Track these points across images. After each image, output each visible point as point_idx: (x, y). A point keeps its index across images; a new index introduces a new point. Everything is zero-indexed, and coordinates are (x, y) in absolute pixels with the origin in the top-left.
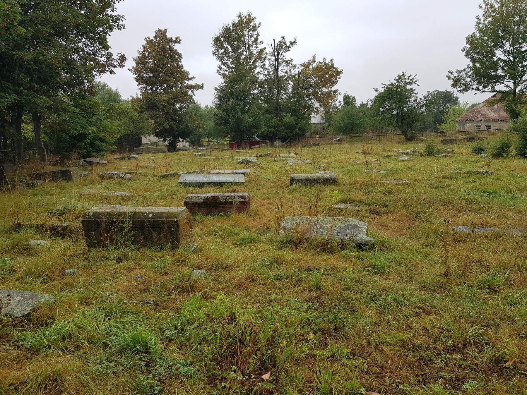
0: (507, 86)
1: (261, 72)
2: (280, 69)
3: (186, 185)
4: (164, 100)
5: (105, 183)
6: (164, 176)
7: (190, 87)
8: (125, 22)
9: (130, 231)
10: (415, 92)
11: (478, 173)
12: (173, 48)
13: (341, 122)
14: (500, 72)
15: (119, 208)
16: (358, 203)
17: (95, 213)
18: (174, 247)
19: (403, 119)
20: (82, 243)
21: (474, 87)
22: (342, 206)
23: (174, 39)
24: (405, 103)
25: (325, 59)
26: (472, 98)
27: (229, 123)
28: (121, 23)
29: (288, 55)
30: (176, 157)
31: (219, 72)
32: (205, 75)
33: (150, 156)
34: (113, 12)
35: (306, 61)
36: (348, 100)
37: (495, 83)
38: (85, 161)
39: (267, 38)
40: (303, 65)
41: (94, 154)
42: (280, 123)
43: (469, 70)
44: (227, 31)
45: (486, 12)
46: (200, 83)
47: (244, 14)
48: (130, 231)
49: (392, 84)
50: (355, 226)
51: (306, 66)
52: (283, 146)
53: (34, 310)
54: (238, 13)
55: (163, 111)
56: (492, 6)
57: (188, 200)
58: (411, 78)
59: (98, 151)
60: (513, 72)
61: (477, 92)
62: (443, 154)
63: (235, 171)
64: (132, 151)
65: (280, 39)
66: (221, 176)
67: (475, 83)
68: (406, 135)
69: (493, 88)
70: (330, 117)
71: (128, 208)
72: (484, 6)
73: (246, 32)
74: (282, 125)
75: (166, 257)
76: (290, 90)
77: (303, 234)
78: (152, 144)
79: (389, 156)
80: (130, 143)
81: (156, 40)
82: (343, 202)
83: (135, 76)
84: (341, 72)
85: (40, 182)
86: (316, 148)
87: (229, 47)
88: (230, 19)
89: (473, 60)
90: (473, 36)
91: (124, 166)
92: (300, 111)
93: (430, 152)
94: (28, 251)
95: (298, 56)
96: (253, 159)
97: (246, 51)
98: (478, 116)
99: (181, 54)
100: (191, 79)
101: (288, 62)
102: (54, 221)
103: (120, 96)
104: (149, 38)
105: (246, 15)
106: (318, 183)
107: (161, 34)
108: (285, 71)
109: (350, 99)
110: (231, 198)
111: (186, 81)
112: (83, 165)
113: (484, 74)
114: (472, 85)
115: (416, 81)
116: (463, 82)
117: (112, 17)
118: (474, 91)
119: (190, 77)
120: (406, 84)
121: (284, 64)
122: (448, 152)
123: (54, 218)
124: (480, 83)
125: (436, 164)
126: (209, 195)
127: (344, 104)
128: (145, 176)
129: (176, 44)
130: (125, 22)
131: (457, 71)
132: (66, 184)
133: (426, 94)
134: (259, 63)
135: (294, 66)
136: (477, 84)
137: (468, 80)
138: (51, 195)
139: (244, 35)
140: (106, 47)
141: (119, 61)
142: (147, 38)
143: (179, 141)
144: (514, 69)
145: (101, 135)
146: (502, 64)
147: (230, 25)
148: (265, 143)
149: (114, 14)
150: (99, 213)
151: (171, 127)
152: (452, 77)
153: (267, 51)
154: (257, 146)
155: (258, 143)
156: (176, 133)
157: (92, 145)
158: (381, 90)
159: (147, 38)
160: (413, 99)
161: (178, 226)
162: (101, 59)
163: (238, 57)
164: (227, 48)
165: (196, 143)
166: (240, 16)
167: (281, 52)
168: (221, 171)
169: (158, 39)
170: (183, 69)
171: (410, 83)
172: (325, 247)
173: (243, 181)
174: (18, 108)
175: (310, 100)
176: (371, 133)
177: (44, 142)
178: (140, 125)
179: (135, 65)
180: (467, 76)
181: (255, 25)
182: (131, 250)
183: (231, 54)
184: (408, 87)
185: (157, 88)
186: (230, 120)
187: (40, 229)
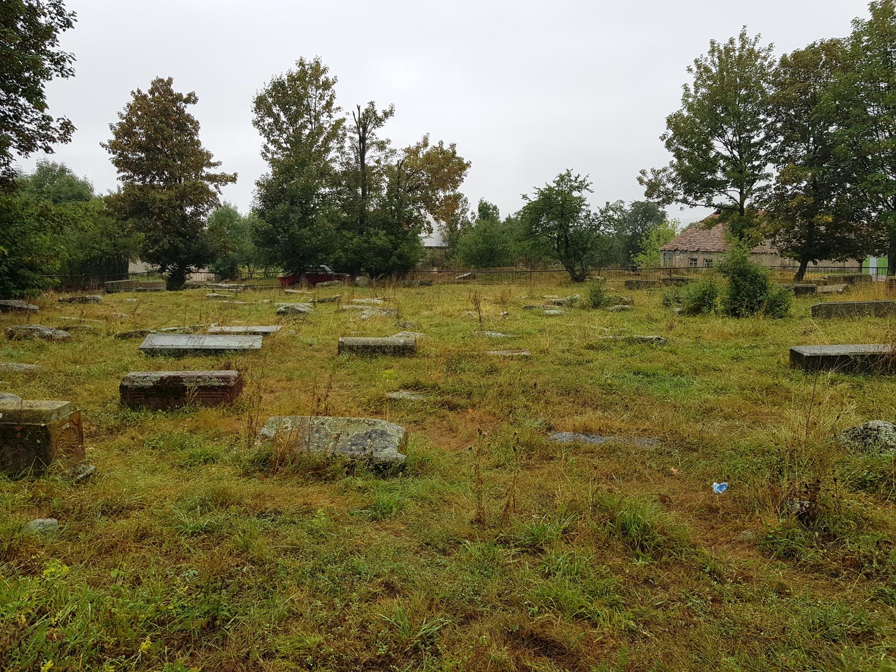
0: (731, 198)
1: (338, 157)
2: (368, 155)
3: (152, 352)
4: (161, 200)
6: (124, 336)
7: (212, 178)
8: (74, 66)
10: (586, 203)
11: (644, 341)
12: (183, 112)
13: (473, 247)
14: (719, 175)
16: (429, 389)
18: (38, 474)
19: (567, 246)
21: (680, 197)
22: (404, 394)
23: (185, 96)
24: (572, 220)
25: (441, 143)
26: (684, 215)
27: (278, 242)
29: (380, 133)
31: (264, 155)
32: (239, 161)
34: (53, 46)
35: (413, 145)
36: (486, 211)
37: (711, 192)
39: (347, 104)
40: (408, 150)
42: (366, 245)
43: (672, 170)
44: (278, 86)
45: (698, 79)
46: (230, 173)
47: (309, 60)
50: (383, 434)
51: (412, 152)
52: (370, 285)
54: (298, 59)
56: (707, 70)
57: (126, 383)
58: (579, 180)
60: (738, 175)
61: (684, 205)
63: (250, 329)
65: (367, 106)
67: (682, 192)
68: (572, 272)
69: (709, 199)
70: (457, 239)
72: (695, 69)
73: (312, 91)
74: (370, 249)
76: (384, 192)
77: (291, 447)
79: (531, 307)
80: (100, 270)
81: (154, 95)
82: (406, 387)
84: (468, 165)
86: (423, 290)
87: (282, 114)
88: (284, 67)
89: (679, 155)
90: (678, 115)
92: (401, 227)
93: (597, 302)
95: (399, 137)
96: (302, 306)
97: (311, 123)
98: (694, 244)
99: (198, 122)
100: (215, 165)
101: (381, 146)
103: (92, 190)
104: (139, 91)
105: (312, 62)
106: (384, 353)
107: (162, 87)
108: (377, 158)
109: (489, 209)
110: (205, 381)
111: (205, 168)
113: (695, 179)
114: (677, 194)
115: (588, 185)
116: (662, 189)
118: (680, 204)
119: (212, 161)
120: (572, 188)
121: (375, 147)
122: (625, 303)
124: (688, 191)
125: (598, 325)
126: (165, 374)
128: (96, 335)
129: (188, 105)
131: (653, 171)
133: (603, 206)
134: (333, 144)
135: (393, 152)
136: (685, 193)
137: (670, 186)
139: (307, 95)
140: (41, 106)
141: (62, 132)
142: (135, 91)
143: (190, 271)
144: (741, 172)
146: (722, 163)
147: (285, 77)
148: (339, 278)
151: (176, 248)
152: (646, 180)
154: (325, 283)
155: (329, 278)
158: (534, 198)
159: (135, 91)
160: (584, 214)
161: (48, 436)
162: (30, 127)
163: (298, 132)
164: (278, 115)
165: (227, 273)
166: (301, 64)
167: (369, 128)
168: (227, 329)
169: (157, 94)
170: (202, 147)
171: (579, 188)
172: (320, 472)
175: (418, 209)
176: (521, 267)
178: (121, 241)
180: (669, 180)
181: (327, 79)
183: (285, 126)
184: (575, 194)
185: (154, 178)
186: (279, 237)
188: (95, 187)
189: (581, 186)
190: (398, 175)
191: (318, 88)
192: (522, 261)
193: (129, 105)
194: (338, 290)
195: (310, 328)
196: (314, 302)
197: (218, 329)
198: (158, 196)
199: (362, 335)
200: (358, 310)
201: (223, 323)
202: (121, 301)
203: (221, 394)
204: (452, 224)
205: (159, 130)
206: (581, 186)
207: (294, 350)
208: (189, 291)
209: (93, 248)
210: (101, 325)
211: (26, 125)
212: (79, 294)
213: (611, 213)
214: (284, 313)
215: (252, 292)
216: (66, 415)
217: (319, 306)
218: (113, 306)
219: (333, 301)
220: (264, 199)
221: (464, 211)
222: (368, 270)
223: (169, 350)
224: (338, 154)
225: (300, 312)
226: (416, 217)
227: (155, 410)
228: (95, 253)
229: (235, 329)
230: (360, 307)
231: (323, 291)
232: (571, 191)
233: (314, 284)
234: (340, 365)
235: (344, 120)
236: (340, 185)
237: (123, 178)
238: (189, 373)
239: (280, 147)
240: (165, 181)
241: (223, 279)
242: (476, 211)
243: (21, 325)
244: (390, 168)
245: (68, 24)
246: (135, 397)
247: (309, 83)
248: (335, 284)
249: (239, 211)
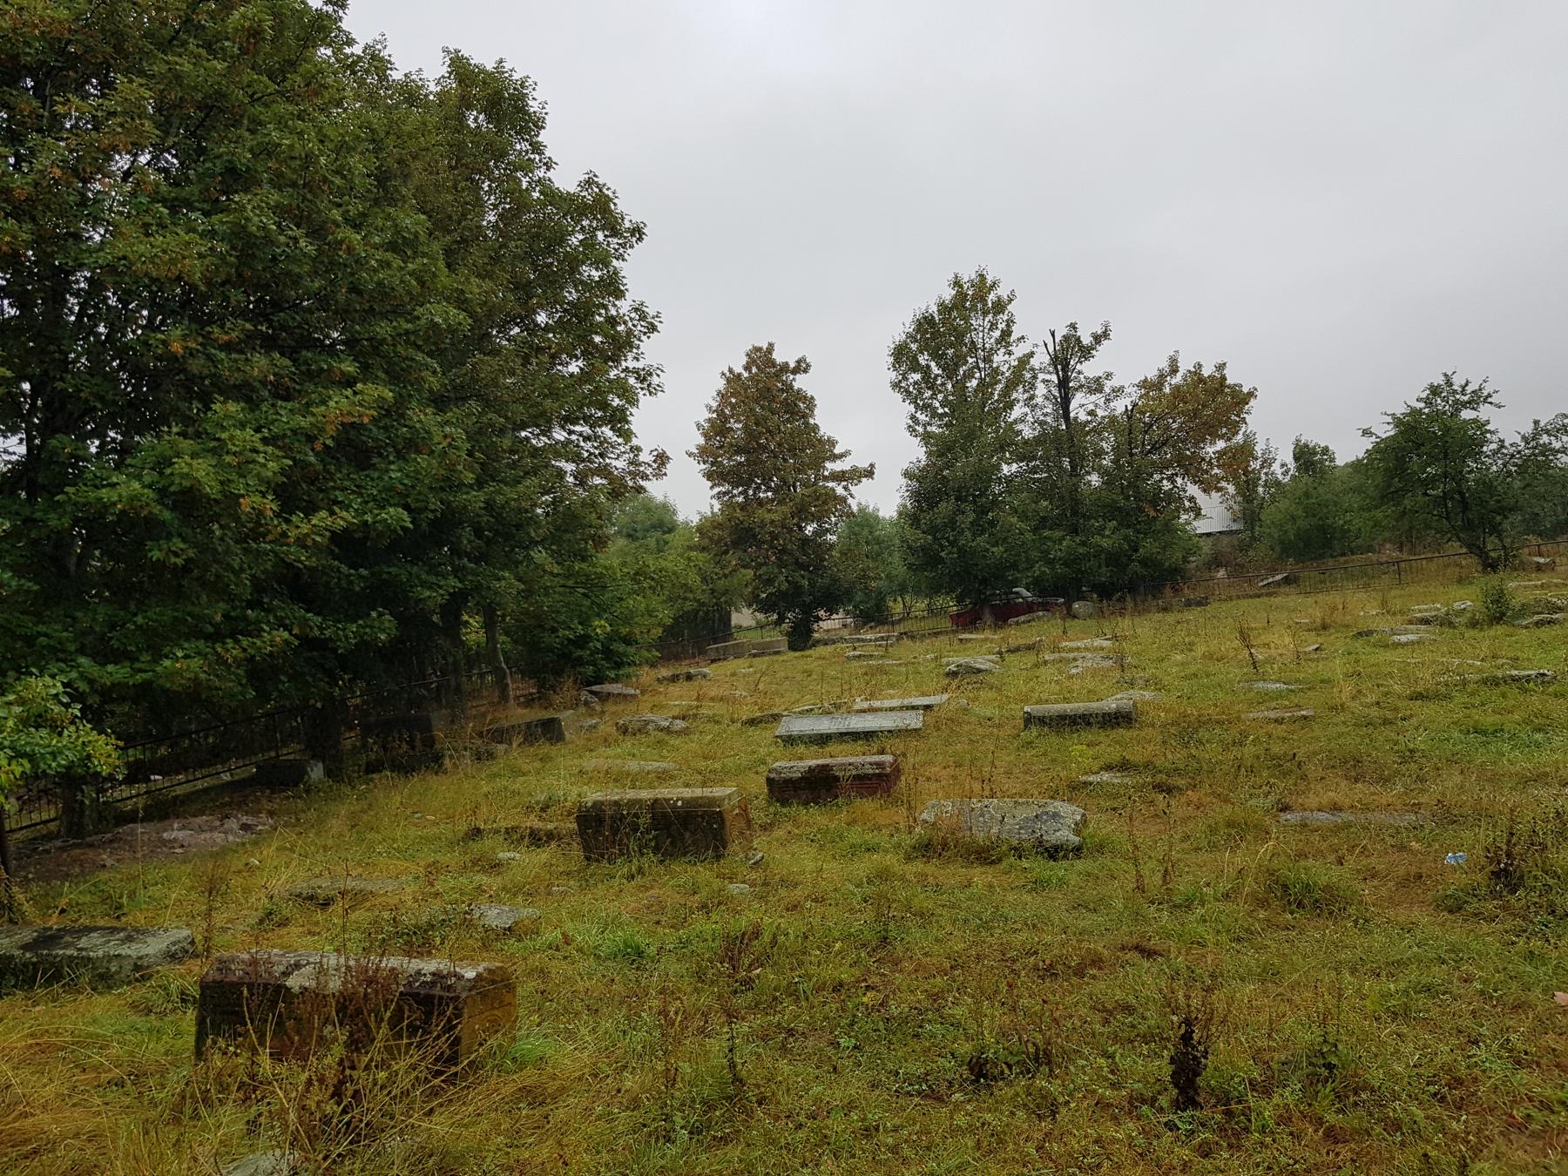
1: (1027, 416)
2: (1073, 405)
3: (790, 740)
4: (773, 522)
5: (628, 744)
6: (752, 722)
7: (839, 477)
9: (648, 831)
12: (791, 387)
15: (631, 794)
17: (595, 804)
18: (718, 857)
20: (577, 852)
22: (1106, 776)
23: (792, 365)
27: (942, 560)
28: (655, 380)
29: (1089, 369)
32: (876, 446)
35: (1152, 374)
36: (1307, 457)
38: (591, 692)
39: (1035, 329)
40: (1145, 384)
41: (612, 674)
44: (925, 324)
46: (863, 464)
48: (648, 831)
49: (1415, 412)
50: (1056, 815)
51: (1150, 386)
53: (516, 923)
55: (772, 547)
59: (618, 665)
62: (1536, 618)
63: (906, 702)
65: (1065, 331)
66: (869, 717)
71: (645, 794)
75: (703, 873)
80: (698, 633)
82: (1109, 768)
83: (703, 466)
84: (1251, 394)
85: (502, 747)
87: (933, 364)
88: (932, 294)
92: (1141, 510)
94: (496, 867)
95: (1125, 368)
96: (981, 662)
100: (841, 456)
101: (1096, 386)
102: (533, 822)
103: (674, 512)
104: (731, 370)
106: (1089, 724)
107: (761, 358)
109: (1315, 454)
112: (586, 703)
115: (1489, 396)
117: (636, 371)
119: (837, 451)
120: (1459, 406)
123: (532, 817)
126: (813, 763)
127: (1298, 469)
128: (717, 722)
130: (664, 379)
133: (1528, 429)
134: (1019, 394)
135: (1118, 391)
138: (524, 774)
140: (627, 435)
143: (818, 619)
145: (624, 631)
148: (1045, 607)
149: (639, 365)
150: (602, 803)
153: (1035, 362)
154: (1022, 618)
155: (1029, 608)
156: (808, 599)
157: (608, 653)
158: (1386, 431)
161: (723, 820)
163: (960, 387)
164: (928, 366)
165: (873, 615)
166: (957, 283)
168: (877, 704)
169: (754, 370)
172: (984, 855)
173: (919, 725)
174: (457, 602)
175: (1171, 479)
176: (1390, 552)
177: (505, 653)
179: (702, 441)
182: (649, 860)
184: (1467, 414)
187: (512, 836)
188: (679, 508)
189: (1477, 399)
190: (1129, 427)
191: (985, 314)
192: (1390, 541)
193: (719, 393)
194: (1041, 629)
195: (992, 694)
196: (1000, 653)
197: (865, 705)
198: (768, 517)
199: (1066, 700)
200: (1068, 661)
201: (872, 696)
202: (734, 674)
203: (877, 783)
204: (1247, 488)
205: (765, 420)
206: (1477, 399)
207: (966, 728)
208: (821, 650)
209: (685, 599)
210: (719, 709)
211: (614, 463)
212: (683, 668)
213: (1545, 439)
214: (954, 674)
216: (735, 801)
217: (1009, 658)
218: (727, 679)
219: (1030, 648)
220: (917, 496)
221: (1267, 463)
222: (1095, 587)
223: (810, 737)
224: (1027, 410)
225: (979, 671)
226: (1169, 494)
227: (806, 804)
228: (689, 606)
229: (887, 704)
230: (1071, 655)
231: (1016, 634)
232: (1458, 410)
233: (1005, 621)
234: (1029, 744)
235: (1032, 354)
236: (1034, 458)
237: (719, 496)
238: (839, 760)
239: (934, 414)
240: (775, 491)
241: (865, 624)
242: (1290, 460)
243: (627, 715)
244: (1113, 419)
245: (652, 328)
246: (784, 790)
247: (970, 310)
248: (1039, 618)
249: (881, 514)
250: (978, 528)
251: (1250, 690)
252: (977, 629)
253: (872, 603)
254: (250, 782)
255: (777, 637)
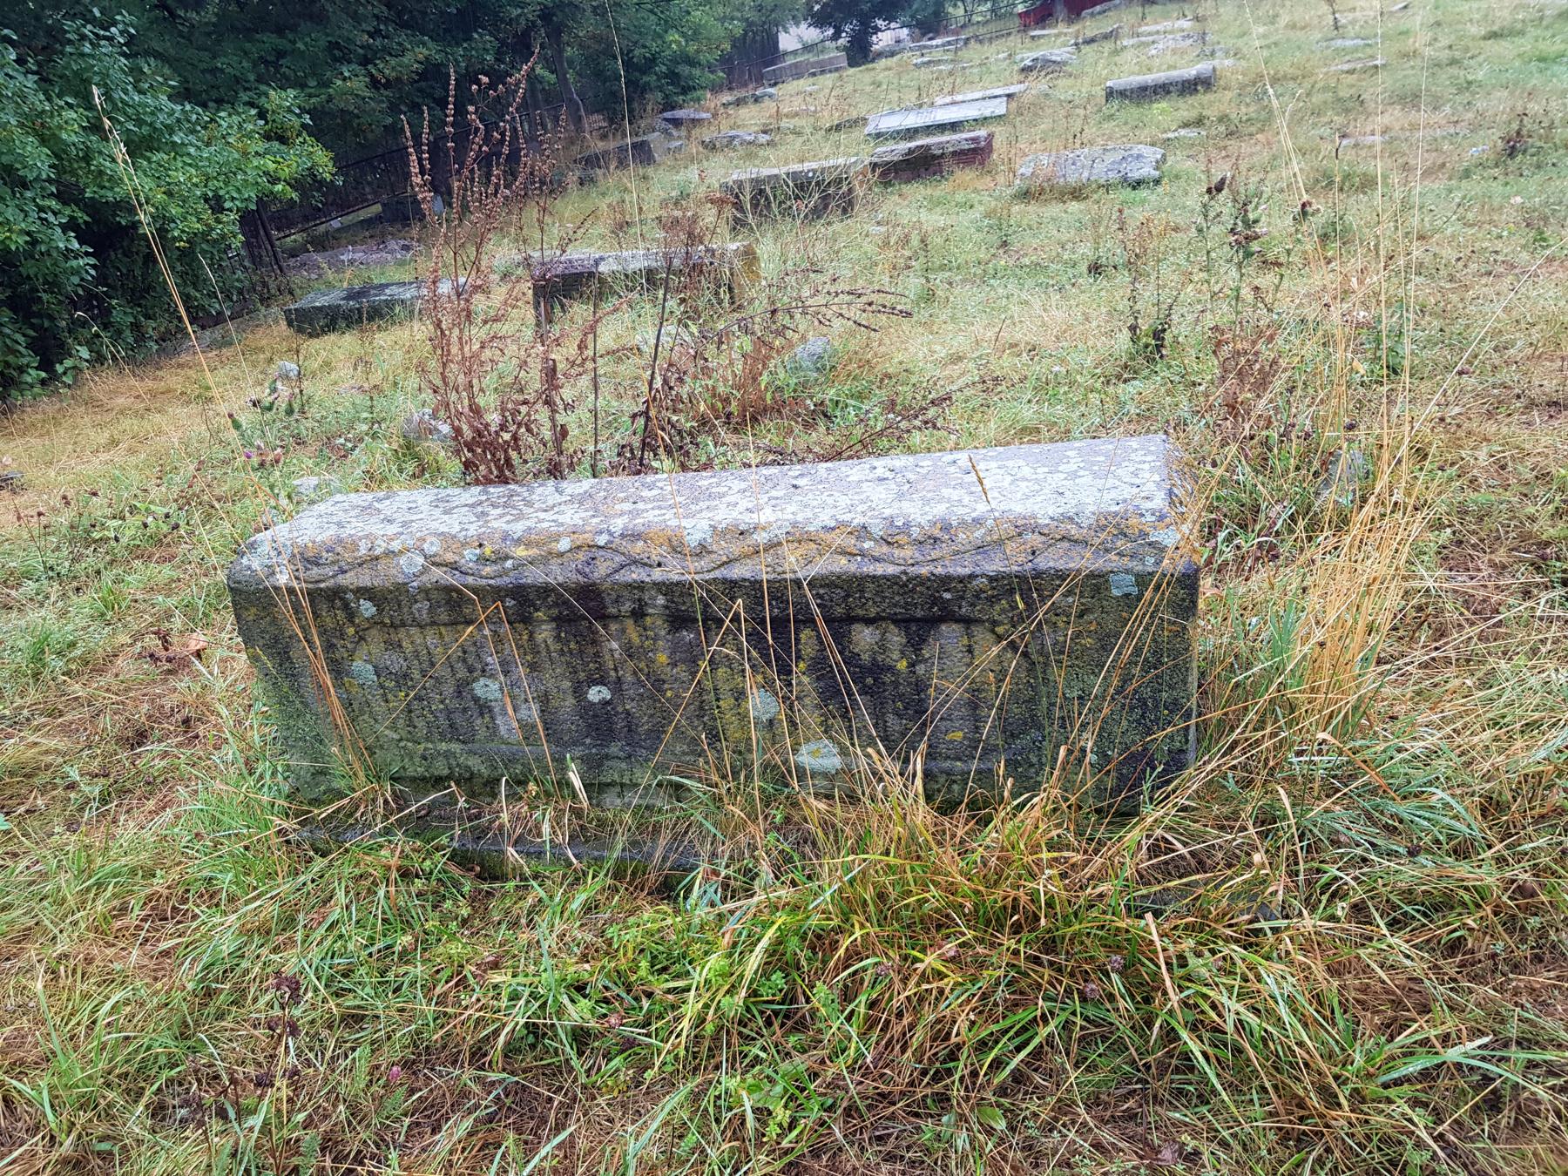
22: (1183, 132)
30: (867, 78)
33: (804, 84)
59: (685, 90)
64: (759, 80)
66: (954, 108)
78: (808, 48)
82: (1186, 125)
85: (599, 172)
91: (750, 118)
132: (650, 171)
143: (877, 30)
145: (692, 48)
154: (1098, 8)
157: (673, 77)
168: (959, 98)
195: (1071, 81)
196: (1076, 44)
197: (948, 99)
203: (975, 155)
215: (978, 46)
217: (1086, 49)
219: (1106, 37)
227: (908, 181)
229: (970, 96)
230: (1150, 39)
233: (1078, 14)
241: (924, 35)
250: (1026, 1093)
251: (1327, 48)
252: (1050, 26)
253: (930, 10)
254: (378, 219)
255: (834, 52)
